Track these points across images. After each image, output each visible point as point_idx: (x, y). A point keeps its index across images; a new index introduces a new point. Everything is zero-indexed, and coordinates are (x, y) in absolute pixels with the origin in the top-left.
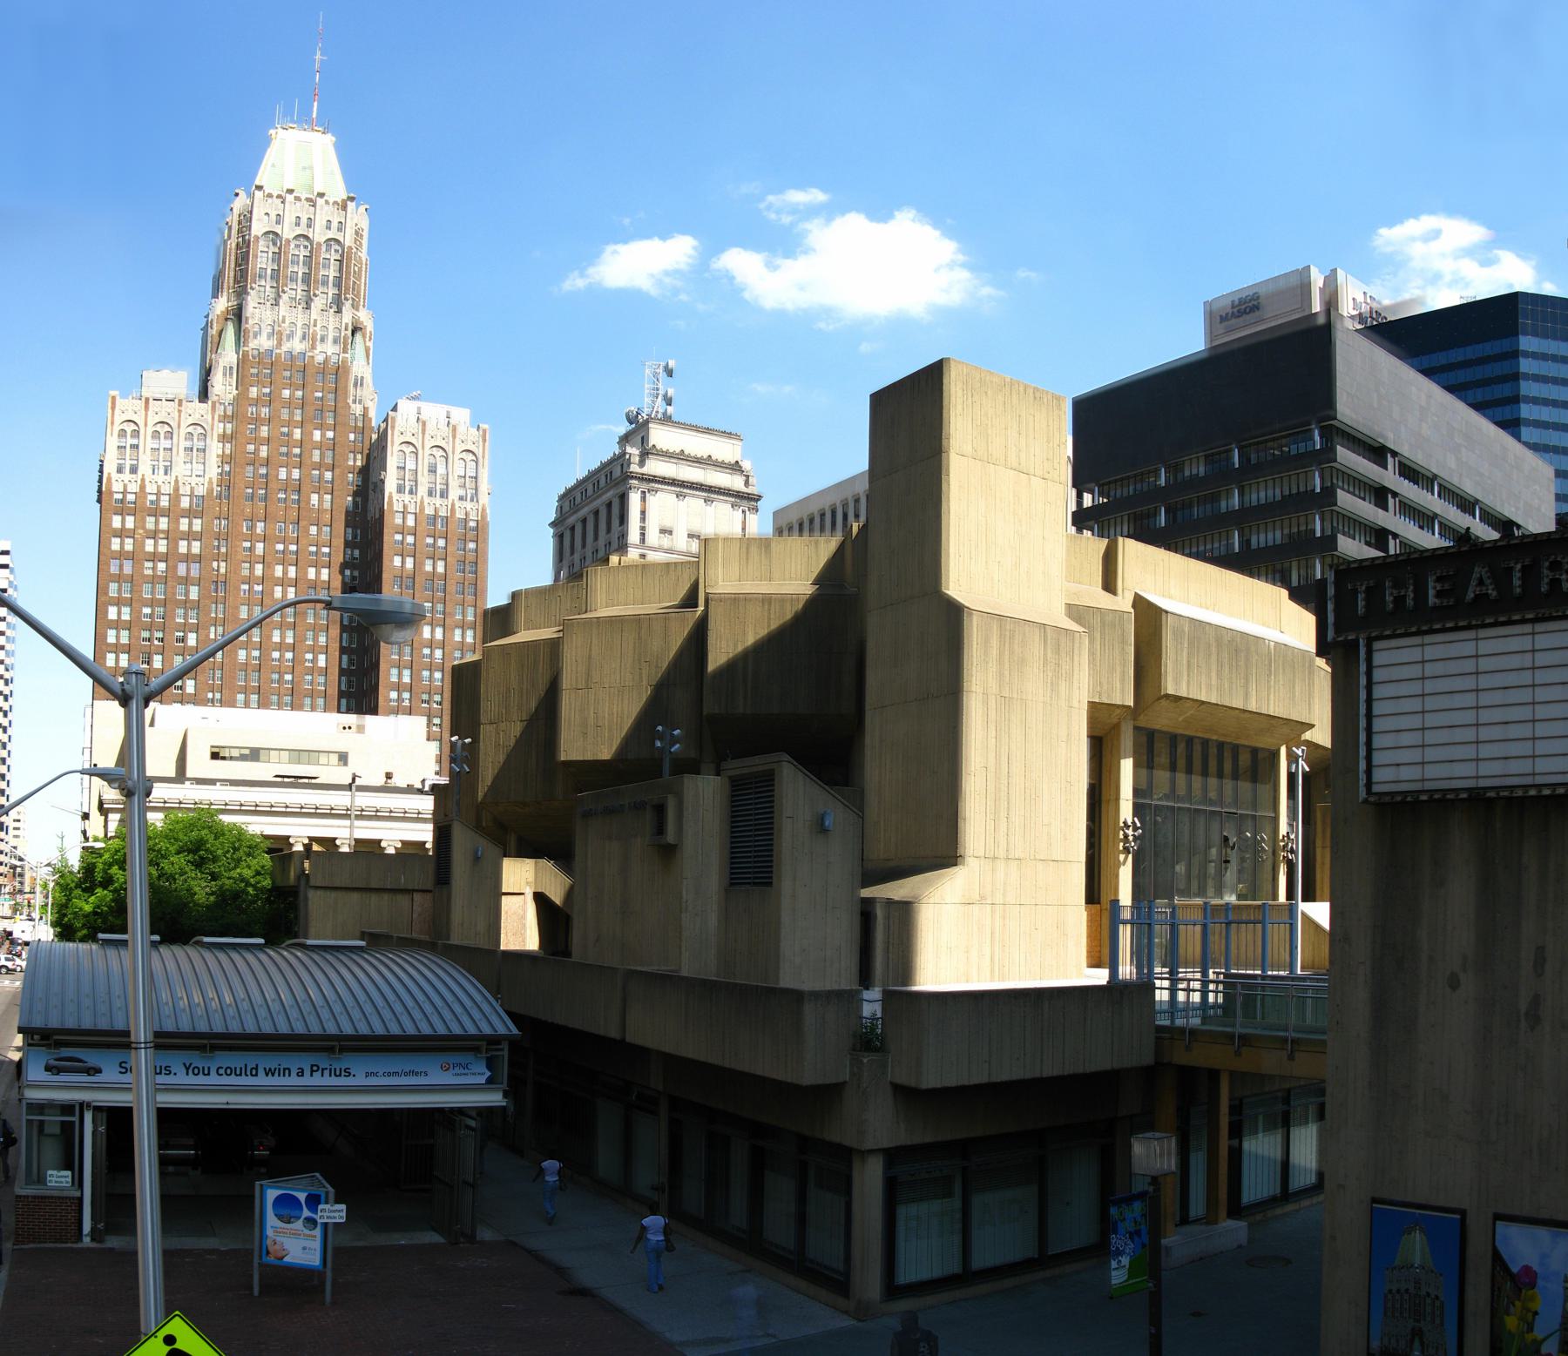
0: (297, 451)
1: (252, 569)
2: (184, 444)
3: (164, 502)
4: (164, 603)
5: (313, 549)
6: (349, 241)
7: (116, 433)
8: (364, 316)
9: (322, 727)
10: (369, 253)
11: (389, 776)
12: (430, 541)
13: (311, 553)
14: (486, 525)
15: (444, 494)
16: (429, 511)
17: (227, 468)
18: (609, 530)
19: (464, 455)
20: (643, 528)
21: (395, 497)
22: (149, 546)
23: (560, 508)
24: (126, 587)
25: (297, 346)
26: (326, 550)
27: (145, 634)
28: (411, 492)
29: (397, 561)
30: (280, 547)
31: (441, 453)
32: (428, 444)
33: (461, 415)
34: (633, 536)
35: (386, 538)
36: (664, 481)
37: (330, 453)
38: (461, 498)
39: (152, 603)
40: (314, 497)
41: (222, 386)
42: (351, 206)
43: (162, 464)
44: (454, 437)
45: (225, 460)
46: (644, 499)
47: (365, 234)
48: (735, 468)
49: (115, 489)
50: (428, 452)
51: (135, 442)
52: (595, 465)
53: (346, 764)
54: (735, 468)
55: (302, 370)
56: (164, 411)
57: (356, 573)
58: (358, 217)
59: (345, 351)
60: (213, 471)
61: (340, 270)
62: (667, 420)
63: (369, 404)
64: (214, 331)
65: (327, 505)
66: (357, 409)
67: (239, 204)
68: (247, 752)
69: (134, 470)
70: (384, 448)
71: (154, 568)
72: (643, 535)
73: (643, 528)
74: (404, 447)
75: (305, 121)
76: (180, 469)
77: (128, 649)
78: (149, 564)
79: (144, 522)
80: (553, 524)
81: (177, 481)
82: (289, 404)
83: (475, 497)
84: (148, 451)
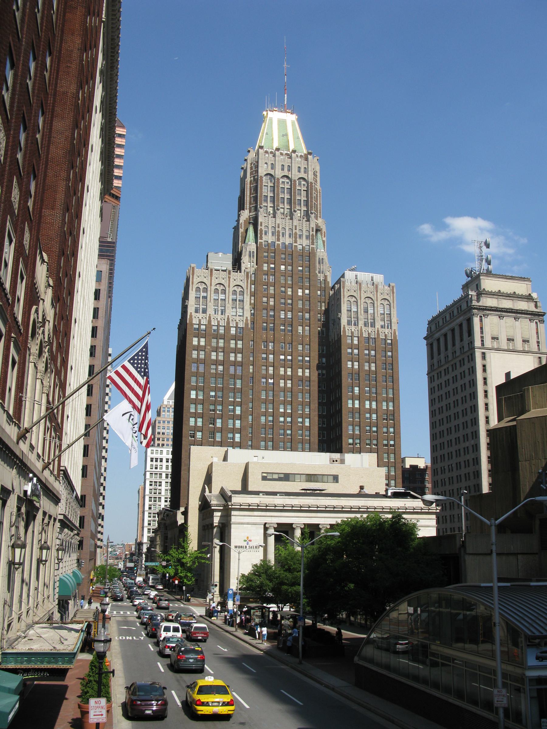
0: (290, 301)
1: (267, 370)
2: (231, 297)
3: (222, 331)
4: (222, 389)
5: (300, 358)
6: (311, 178)
7: (194, 289)
8: (320, 221)
9: (319, 461)
10: (321, 186)
11: (362, 488)
12: (366, 352)
13: (299, 361)
14: (397, 341)
15: (373, 325)
16: (365, 335)
17: (253, 312)
18: (462, 340)
19: (383, 302)
20: (482, 337)
22: (213, 356)
23: (429, 329)
24: (201, 379)
25: (288, 241)
26: (307, 359)
27: (212, 407)
28: (355, 325)
29: (349, 364)
30: (282, 357)
31: (370, 301)
32: (363, 296)
33: (379, 278)
34: (477, 343)
35: (343, 351)
37: (307, 303)
38: (382, 327)
39: (215, 389)
40: (300, 328)
41: (247, 263)
42: (310, 157)
43: (220, 308)
44: (377, 291)
45: (254, 307)
46: (481, 320)
47: (318, 174)
48: (529, 298)
49: (194, 322)
50: (363, 300)
51: (205, 294)
52: (450, 303)
53: (337, 482)
54: (529, 298)
55: (290, 254)
56: (221, 278)
57: (324, 372)
58: (314, 164)
59: (313, 244)
60: (248, 314)
61: (307, 196)
62: (489, 273)
63: (328, 274)
64: (241, 230)
65: (307, 333)
66: (321, 277)
67: (251, 156)
68: (282, 476)
69: (204, 311)
70: (339, 300)
71: (216, 369)
72: (482, 341)
74: (350, 298)
75: (283, 108)
76: (230, 312)
77: (202, 416)
78: (213, 367)
79: (211, 342)
80: (425, 338)
81: (228, 319)
82: (284, 274)
83: (390, 326)
84: (212, 301)
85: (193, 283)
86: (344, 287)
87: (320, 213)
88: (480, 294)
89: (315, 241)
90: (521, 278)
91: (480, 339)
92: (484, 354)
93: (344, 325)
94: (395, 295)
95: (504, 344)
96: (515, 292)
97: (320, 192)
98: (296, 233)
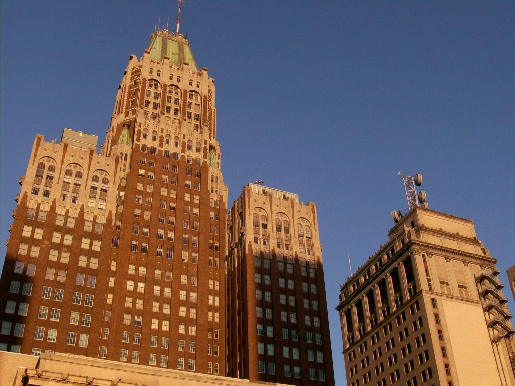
7: (36, 164)
10: (216, 106)
20: (429, 280)
21: (254, 246)
25: (172, 149)
36: (435, 247)
45: (120, 202)
48: (474, 241)
50: (275, 216)
69: (46, 194)
72: (429, 285)
73: (429, 280)
76: (83, 198)
85: (35, 156)
86: (249, 196)
87: (214, 133)
88: (419, 229)
89: (208, 155)
90: (462, 219)
91: (427, 282)
92: (433, 300)
93: (250, 242)
94: (316, 215)
95: (456, 291)
96: (458, 233)
97: (214, 113)
98: (184, 143)
